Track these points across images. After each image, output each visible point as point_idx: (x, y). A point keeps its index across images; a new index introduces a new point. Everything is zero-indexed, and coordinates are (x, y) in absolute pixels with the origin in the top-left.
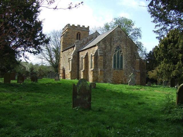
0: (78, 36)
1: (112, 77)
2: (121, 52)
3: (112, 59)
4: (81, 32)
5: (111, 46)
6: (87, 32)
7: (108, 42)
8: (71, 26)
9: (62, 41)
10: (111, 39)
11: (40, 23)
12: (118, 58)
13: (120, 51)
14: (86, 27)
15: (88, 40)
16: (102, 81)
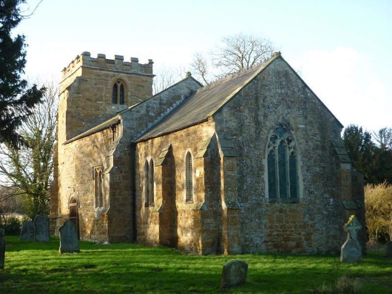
0: (119, 93)
1: (268, 231)
2: (289, 141)
3: (261, 169)
4: (128, 82)
5: (258, 123)
6: (145, 78)
7: (247, 111)
8: (93, 60)
9: (65, 109)
10: (257, 99)
11: (20, 41)
12: (282, 164)
13: (288, 139)
14: (143, 61)
15: (164, 104)
16: (236, 245)
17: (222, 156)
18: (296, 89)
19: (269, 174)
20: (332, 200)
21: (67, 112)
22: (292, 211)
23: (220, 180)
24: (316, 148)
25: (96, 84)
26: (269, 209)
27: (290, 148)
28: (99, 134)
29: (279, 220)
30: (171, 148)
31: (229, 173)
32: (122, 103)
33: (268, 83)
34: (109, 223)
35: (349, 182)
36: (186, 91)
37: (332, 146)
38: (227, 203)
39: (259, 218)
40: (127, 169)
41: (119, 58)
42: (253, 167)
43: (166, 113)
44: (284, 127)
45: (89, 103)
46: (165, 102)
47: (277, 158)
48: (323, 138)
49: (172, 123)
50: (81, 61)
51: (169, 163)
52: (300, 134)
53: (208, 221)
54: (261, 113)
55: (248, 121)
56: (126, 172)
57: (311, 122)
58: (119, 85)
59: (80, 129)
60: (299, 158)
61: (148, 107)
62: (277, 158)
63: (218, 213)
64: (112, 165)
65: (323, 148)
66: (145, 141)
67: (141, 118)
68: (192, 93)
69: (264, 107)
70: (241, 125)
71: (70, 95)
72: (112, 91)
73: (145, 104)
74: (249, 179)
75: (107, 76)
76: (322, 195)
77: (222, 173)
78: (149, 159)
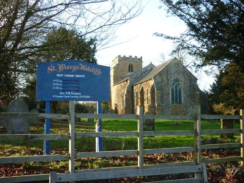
0: (131, 68)
2: (179, 85)
3: (169, 93)
4: (134, 65)
7: (164, 76)
10: (168, 72)
13: (178, 84)
14: (139, 57)
17: (156, 90)
18: (181, 68)
19: (172, 95)
20: (193, 103)
21: (114, 76)
22: (179, 106)
23: (155, 97)
24: (188, 86)
25: (123, 66)
26: (172, 106)
27: (179, 87)
28: (122, 83)
29: (175, 109)
30: (143, 87)
31: (158, 95)
32: (132, 72)
33: (171, 67)
34: (125, 111)
35: (199, 97)
36: (150, 68)
37: (193, 86)
38: (157, 104)
39: (168, 108)
40: (131, 94)
41: (131, 57)
42: (166, 93)
43: (143, 76)
44: (177, 80)
45: (121, 72)
46: (143, 72)
47: (174, 90)
48: (191, 83)
49: (143, 80)
50: (118, 59)
51: (142, 92)
52: (182, 82)
53: (152, 109)
54: (169, 76)
55: (165, 79)
56: (131, 95)
57: (186, 78)
58: (131, 66)
59: (118, 81)
60: (182, 90)
61: (137, 74)
62: (174, 90)
63: (154, 107)
64: (126, 93)
65: (191, 87)
66: (135, 85)
67: (135, 78)
68: (152, 69)
69: (170, 74)
70: (162, 81)
71: (114, 70)
72: (128, 68)
73: (136, 73)
74: (165, 97)
75: (127, 63)
76: (190, 101)
77: (156, 95)
78: (137, 91)
